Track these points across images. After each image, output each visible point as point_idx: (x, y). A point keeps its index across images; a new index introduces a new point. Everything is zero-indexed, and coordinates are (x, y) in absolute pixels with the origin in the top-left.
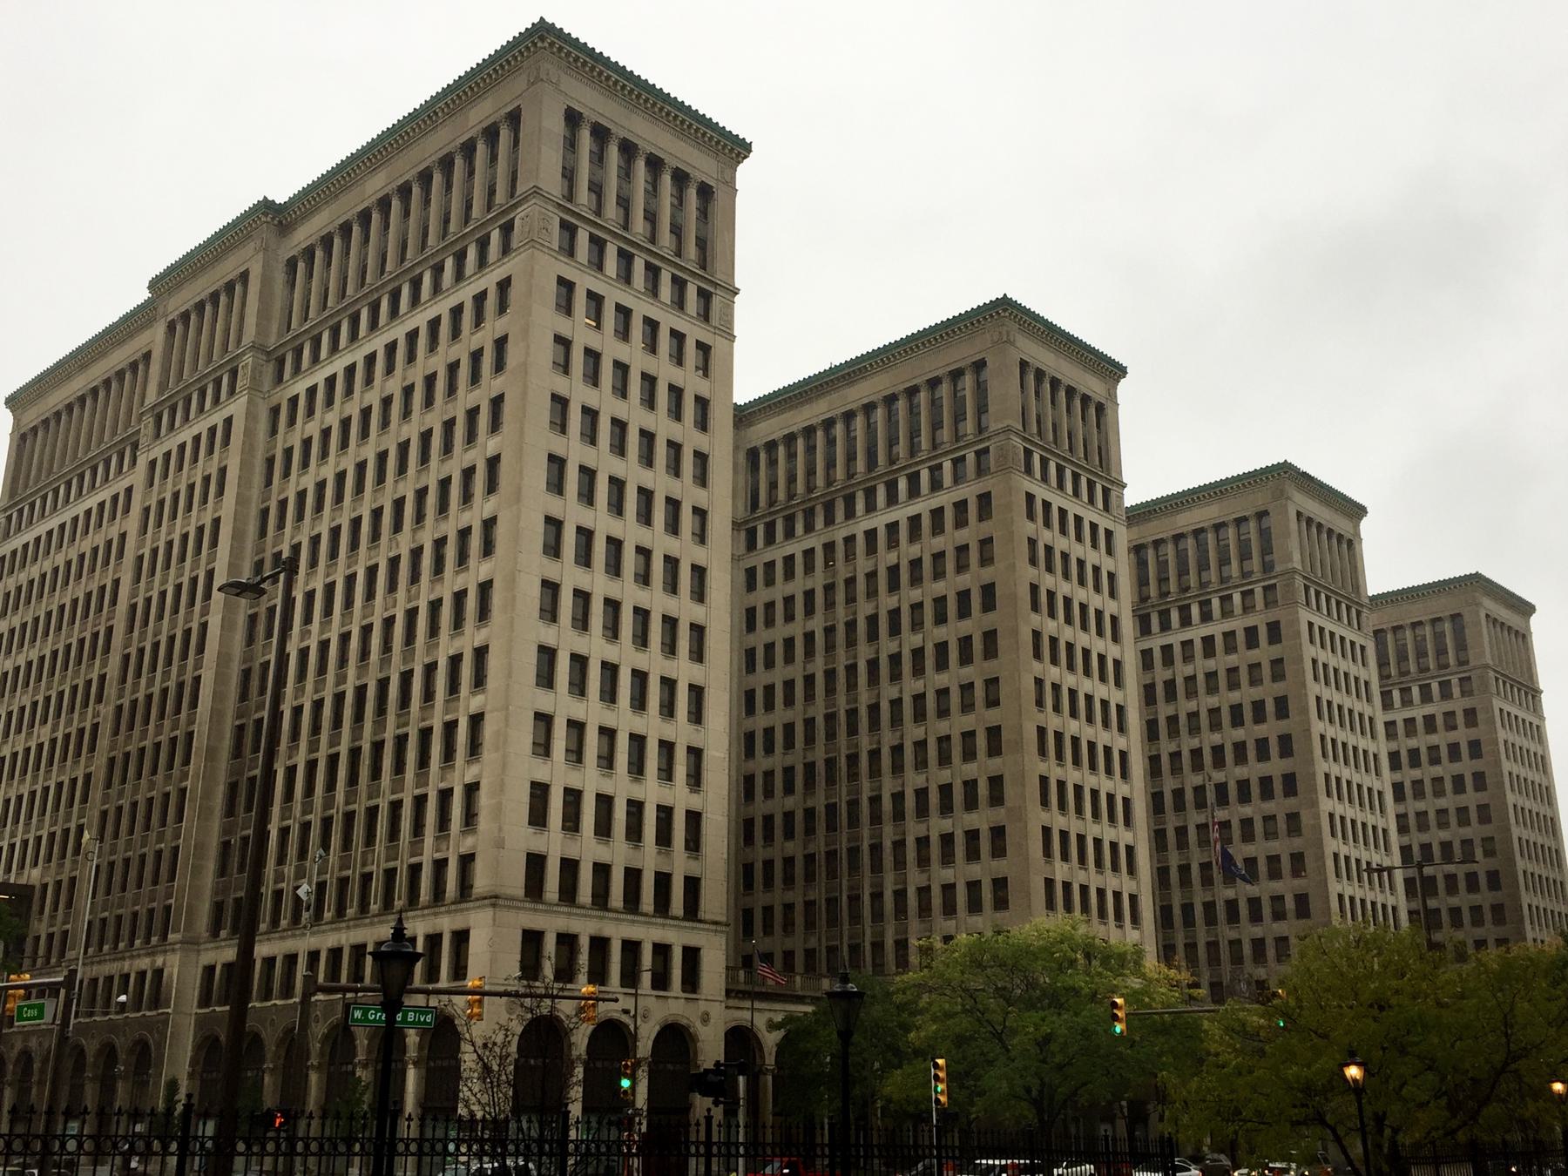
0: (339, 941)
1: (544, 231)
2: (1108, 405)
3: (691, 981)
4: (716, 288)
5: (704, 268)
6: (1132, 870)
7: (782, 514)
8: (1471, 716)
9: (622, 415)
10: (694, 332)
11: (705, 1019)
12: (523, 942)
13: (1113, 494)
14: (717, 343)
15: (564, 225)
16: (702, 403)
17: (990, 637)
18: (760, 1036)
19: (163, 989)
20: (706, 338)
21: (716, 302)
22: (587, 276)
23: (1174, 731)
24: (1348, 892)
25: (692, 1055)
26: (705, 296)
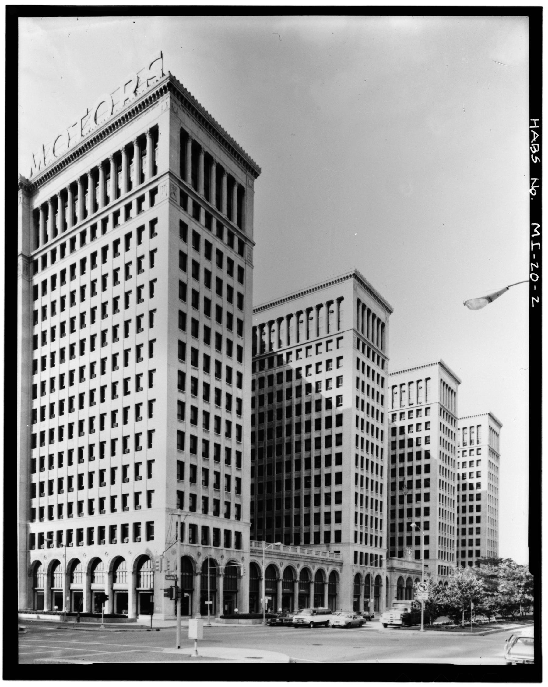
0: (159, 612)
1: (173, 195)
2: (386, 324)
3: (238, 545)
4: (246, 241)
5: (241, 228)
6: (239, 464)
7: (267, 357)
8: (464, 543)
9: (219, 415)
10: (238, 261)
11: (243, 559)
12: (167, 437)
13: (385, 363)
14: (247, 269)
15: (182, 193)
16: (240, 323)
17: (339, 436)
18: (260, 565)
19: (120, 619)
20: (243, 265)
21: (247, 247)
22: (193, 223)
23: (402, 474)
24: (441, 550)
25: (238, 572)
26: (241, 245)
